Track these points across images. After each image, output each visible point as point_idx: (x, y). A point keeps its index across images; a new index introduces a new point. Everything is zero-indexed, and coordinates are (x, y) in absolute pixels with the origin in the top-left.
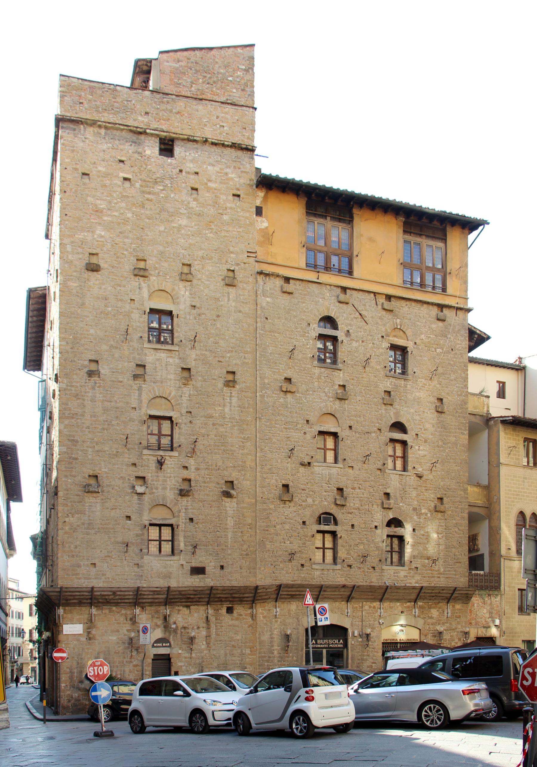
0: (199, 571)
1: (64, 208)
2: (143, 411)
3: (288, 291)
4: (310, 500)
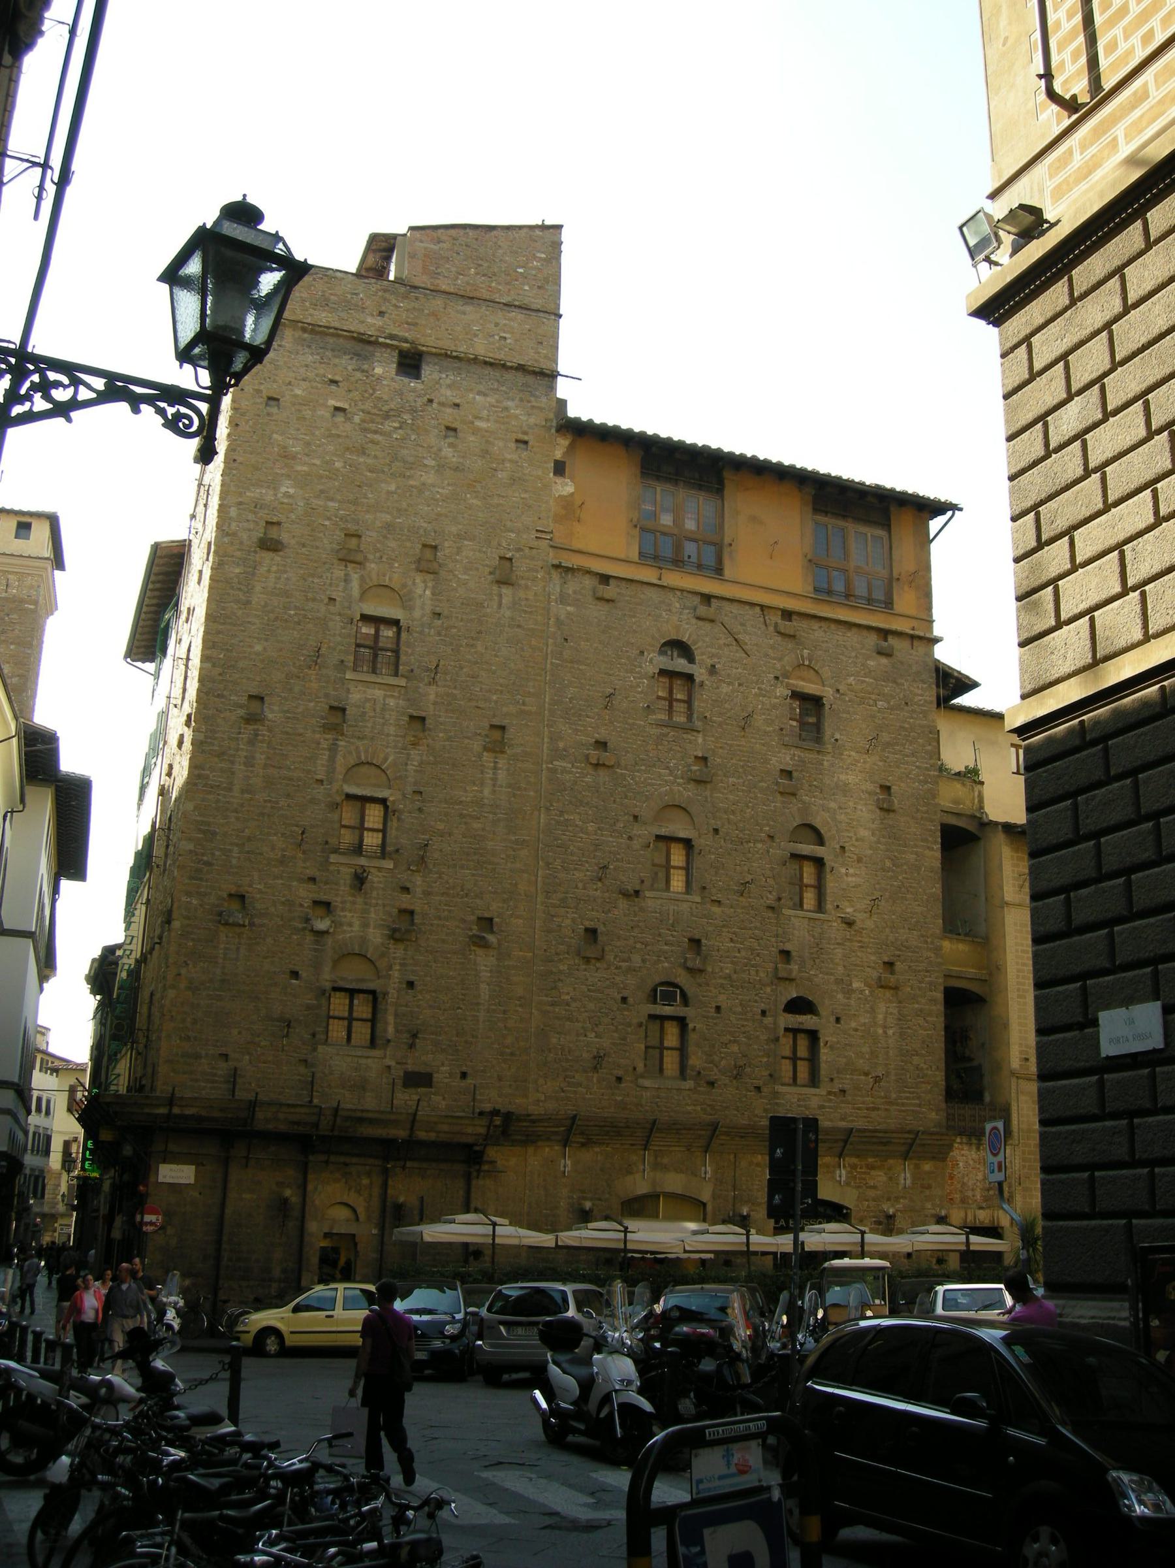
0: (419, 1080)
1: (234, 450)
2: (336, 786)
3: (607, 596)
4: (636, 959)
